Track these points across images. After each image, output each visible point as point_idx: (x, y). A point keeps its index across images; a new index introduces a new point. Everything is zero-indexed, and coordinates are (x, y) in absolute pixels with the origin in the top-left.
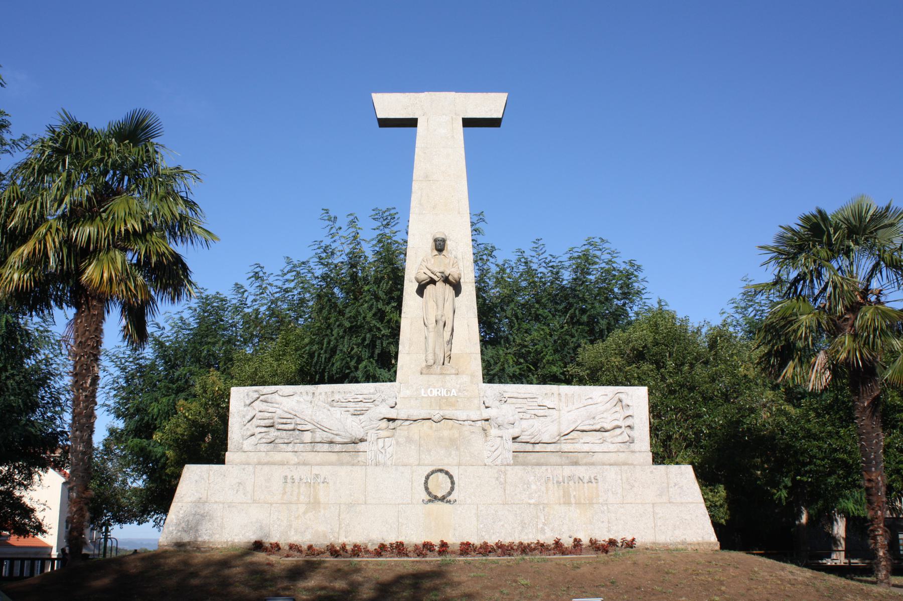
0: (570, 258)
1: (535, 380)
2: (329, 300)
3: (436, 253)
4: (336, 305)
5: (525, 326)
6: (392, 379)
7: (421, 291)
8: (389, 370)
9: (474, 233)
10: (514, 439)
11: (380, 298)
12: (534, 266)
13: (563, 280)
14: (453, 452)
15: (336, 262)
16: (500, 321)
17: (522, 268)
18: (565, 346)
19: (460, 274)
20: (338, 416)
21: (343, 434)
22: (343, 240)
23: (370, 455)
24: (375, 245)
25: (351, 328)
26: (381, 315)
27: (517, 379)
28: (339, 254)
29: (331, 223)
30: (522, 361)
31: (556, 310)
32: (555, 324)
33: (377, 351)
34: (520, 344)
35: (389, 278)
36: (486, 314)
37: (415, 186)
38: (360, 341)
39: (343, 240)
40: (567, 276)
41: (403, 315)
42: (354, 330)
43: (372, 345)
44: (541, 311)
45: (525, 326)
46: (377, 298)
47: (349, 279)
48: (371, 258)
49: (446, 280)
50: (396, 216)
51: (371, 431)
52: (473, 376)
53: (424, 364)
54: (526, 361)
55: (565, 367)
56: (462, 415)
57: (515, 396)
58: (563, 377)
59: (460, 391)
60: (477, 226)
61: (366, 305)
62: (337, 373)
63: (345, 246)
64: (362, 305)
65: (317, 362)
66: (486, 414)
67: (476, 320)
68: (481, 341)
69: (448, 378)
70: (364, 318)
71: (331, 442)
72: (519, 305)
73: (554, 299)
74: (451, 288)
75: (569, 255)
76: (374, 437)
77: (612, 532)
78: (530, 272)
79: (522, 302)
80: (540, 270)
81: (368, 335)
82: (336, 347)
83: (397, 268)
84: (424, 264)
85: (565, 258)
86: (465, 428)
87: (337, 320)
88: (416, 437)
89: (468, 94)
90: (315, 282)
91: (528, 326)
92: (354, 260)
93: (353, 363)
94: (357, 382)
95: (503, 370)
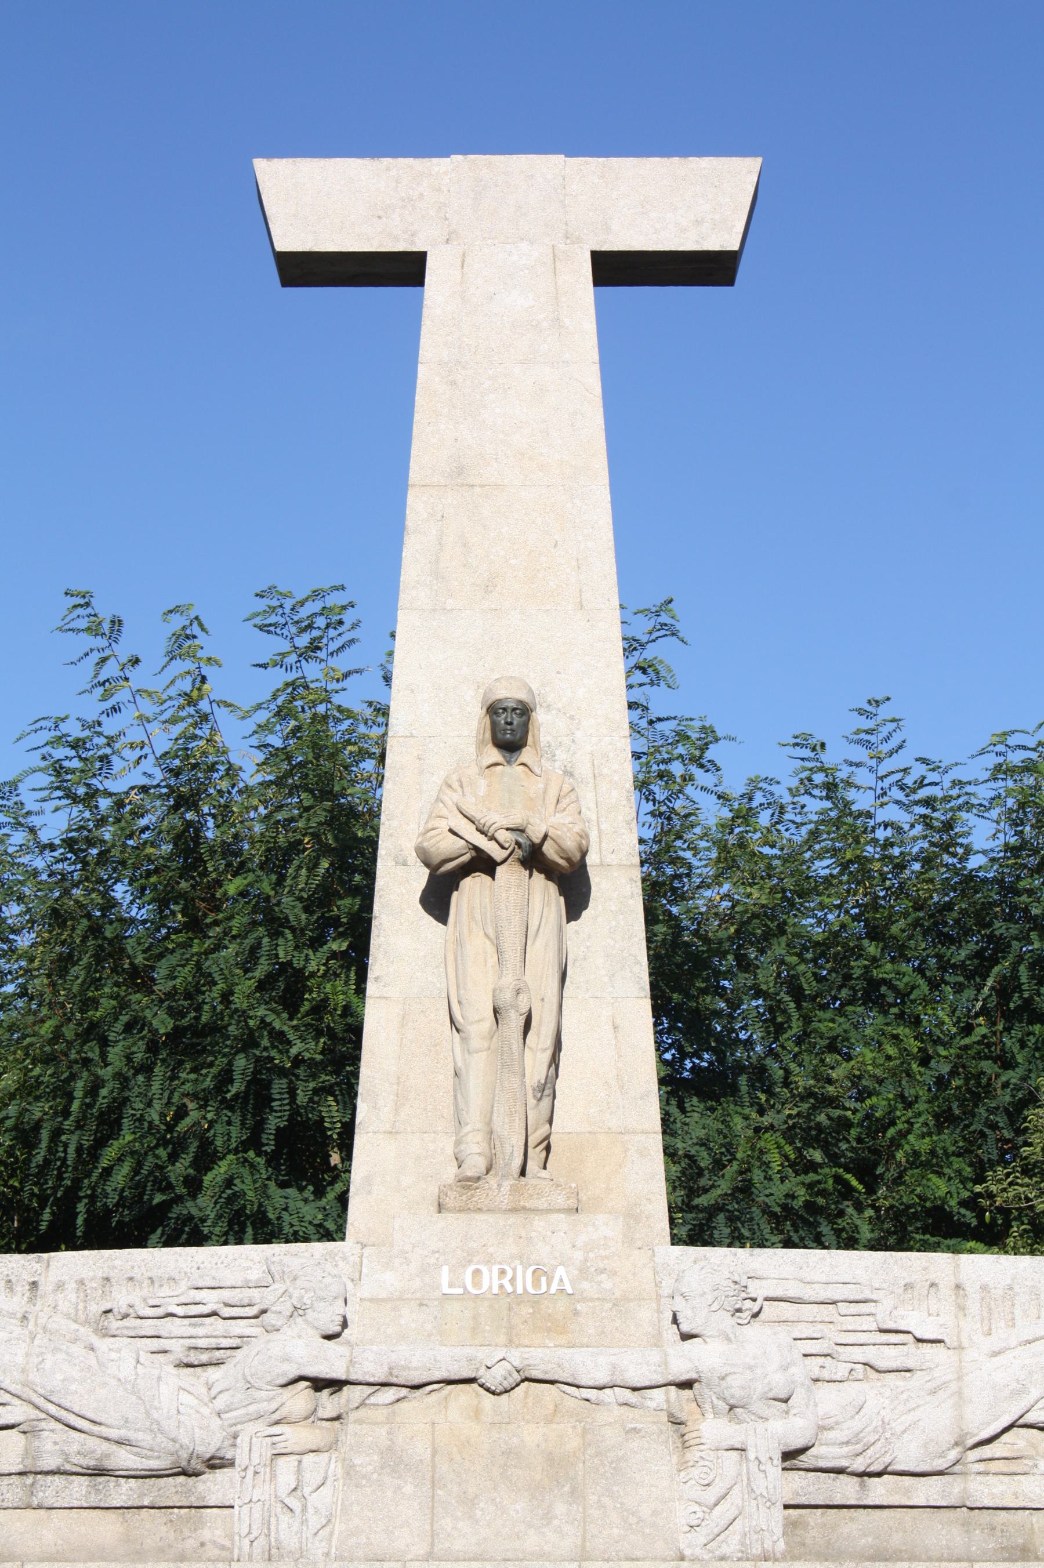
0: (999, 771)
1: (866, 1233)
2: (95, 930)
3: (494, 755)
4: (116, 950)
5: (826, 1024)
6: (331, 1229)
7: (437, 899)
8: (319, 1193)
9: (638, 677)
10: (789, 1455)
11: (285, 922)
12: (862, 801)
13: (968, 851)
14: (560, 1508)
15: (117, 786)
16: (734, 1005)
17: (815, 805)
18: (977, 1098)
19: (584, 835)
20: (126, 1369)
21: (143, 1438)
22: (147, 707)
23: (243, 1520)
24: (263, 728)
25: (177, 1033)
26: (288, 987)
27: (802, 1226)
28: (132, 755)
29: (102, 642)
30: (817, 1156)
31: (944, 965)
32: (941, 1017)
33: (274, 1122)
34: (810, 1094)
35: (324, 850)
36: (681, 977)
37: (418, 506)
38: (208, 1083)
39: (147, 707)
40: (984, 838)
41: (371, 988)
42: (188, 1043)
43: (258, 1095)
44: (886, 970)
45: (826, 1024)
46: (276, 925)
47: (167, 848)
48: (251, 776)
49: (533, 858)
50: (349, 617)
51: (251, 1428)
52: (633, 1216)
53: (450, 1173)
54: (834, 1159)
55: (980, 1179)
56: (592, 1366)
57: (791, 1293)
58: (970, 1217)
59: (584, 1272)
60: (650, 653)
61: (232, 949)
62: (121, 1203)
63: (155, 728)
64: (218, 947)
65: (47, 1162)
66: (683, 1361)
67: (645, 1006)
68: (662, 1082)
69: (539, 1223)
70: (226, 997)
71: (99, 1472)
72: (803, 945)
73: (935, 925)
74: (552, 888)
75: (991, 760)
76: (262, 1450)
77: (1021, 1498)
78: (845, 824)
79: (818, 932)
80: (882, 815)
81: (240, 1062)
82: (119, 1104)
83: (352, 812)
84: (451, 797)
85: (978, 769)
86: (603, 1416)
87: (123, 1005)
88: (421, 1449)
89: (614, 161)
90: (39, 863)
91: (840, 1026)
92: (190, 781)
93: (181, 1168)
94: (197, 1239)
95: (744, 1190)
